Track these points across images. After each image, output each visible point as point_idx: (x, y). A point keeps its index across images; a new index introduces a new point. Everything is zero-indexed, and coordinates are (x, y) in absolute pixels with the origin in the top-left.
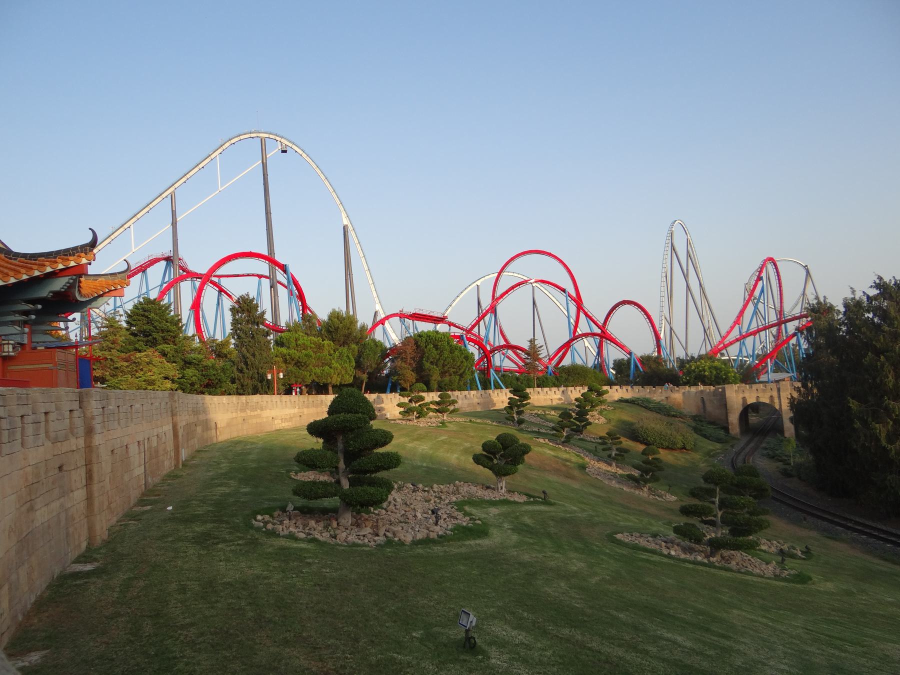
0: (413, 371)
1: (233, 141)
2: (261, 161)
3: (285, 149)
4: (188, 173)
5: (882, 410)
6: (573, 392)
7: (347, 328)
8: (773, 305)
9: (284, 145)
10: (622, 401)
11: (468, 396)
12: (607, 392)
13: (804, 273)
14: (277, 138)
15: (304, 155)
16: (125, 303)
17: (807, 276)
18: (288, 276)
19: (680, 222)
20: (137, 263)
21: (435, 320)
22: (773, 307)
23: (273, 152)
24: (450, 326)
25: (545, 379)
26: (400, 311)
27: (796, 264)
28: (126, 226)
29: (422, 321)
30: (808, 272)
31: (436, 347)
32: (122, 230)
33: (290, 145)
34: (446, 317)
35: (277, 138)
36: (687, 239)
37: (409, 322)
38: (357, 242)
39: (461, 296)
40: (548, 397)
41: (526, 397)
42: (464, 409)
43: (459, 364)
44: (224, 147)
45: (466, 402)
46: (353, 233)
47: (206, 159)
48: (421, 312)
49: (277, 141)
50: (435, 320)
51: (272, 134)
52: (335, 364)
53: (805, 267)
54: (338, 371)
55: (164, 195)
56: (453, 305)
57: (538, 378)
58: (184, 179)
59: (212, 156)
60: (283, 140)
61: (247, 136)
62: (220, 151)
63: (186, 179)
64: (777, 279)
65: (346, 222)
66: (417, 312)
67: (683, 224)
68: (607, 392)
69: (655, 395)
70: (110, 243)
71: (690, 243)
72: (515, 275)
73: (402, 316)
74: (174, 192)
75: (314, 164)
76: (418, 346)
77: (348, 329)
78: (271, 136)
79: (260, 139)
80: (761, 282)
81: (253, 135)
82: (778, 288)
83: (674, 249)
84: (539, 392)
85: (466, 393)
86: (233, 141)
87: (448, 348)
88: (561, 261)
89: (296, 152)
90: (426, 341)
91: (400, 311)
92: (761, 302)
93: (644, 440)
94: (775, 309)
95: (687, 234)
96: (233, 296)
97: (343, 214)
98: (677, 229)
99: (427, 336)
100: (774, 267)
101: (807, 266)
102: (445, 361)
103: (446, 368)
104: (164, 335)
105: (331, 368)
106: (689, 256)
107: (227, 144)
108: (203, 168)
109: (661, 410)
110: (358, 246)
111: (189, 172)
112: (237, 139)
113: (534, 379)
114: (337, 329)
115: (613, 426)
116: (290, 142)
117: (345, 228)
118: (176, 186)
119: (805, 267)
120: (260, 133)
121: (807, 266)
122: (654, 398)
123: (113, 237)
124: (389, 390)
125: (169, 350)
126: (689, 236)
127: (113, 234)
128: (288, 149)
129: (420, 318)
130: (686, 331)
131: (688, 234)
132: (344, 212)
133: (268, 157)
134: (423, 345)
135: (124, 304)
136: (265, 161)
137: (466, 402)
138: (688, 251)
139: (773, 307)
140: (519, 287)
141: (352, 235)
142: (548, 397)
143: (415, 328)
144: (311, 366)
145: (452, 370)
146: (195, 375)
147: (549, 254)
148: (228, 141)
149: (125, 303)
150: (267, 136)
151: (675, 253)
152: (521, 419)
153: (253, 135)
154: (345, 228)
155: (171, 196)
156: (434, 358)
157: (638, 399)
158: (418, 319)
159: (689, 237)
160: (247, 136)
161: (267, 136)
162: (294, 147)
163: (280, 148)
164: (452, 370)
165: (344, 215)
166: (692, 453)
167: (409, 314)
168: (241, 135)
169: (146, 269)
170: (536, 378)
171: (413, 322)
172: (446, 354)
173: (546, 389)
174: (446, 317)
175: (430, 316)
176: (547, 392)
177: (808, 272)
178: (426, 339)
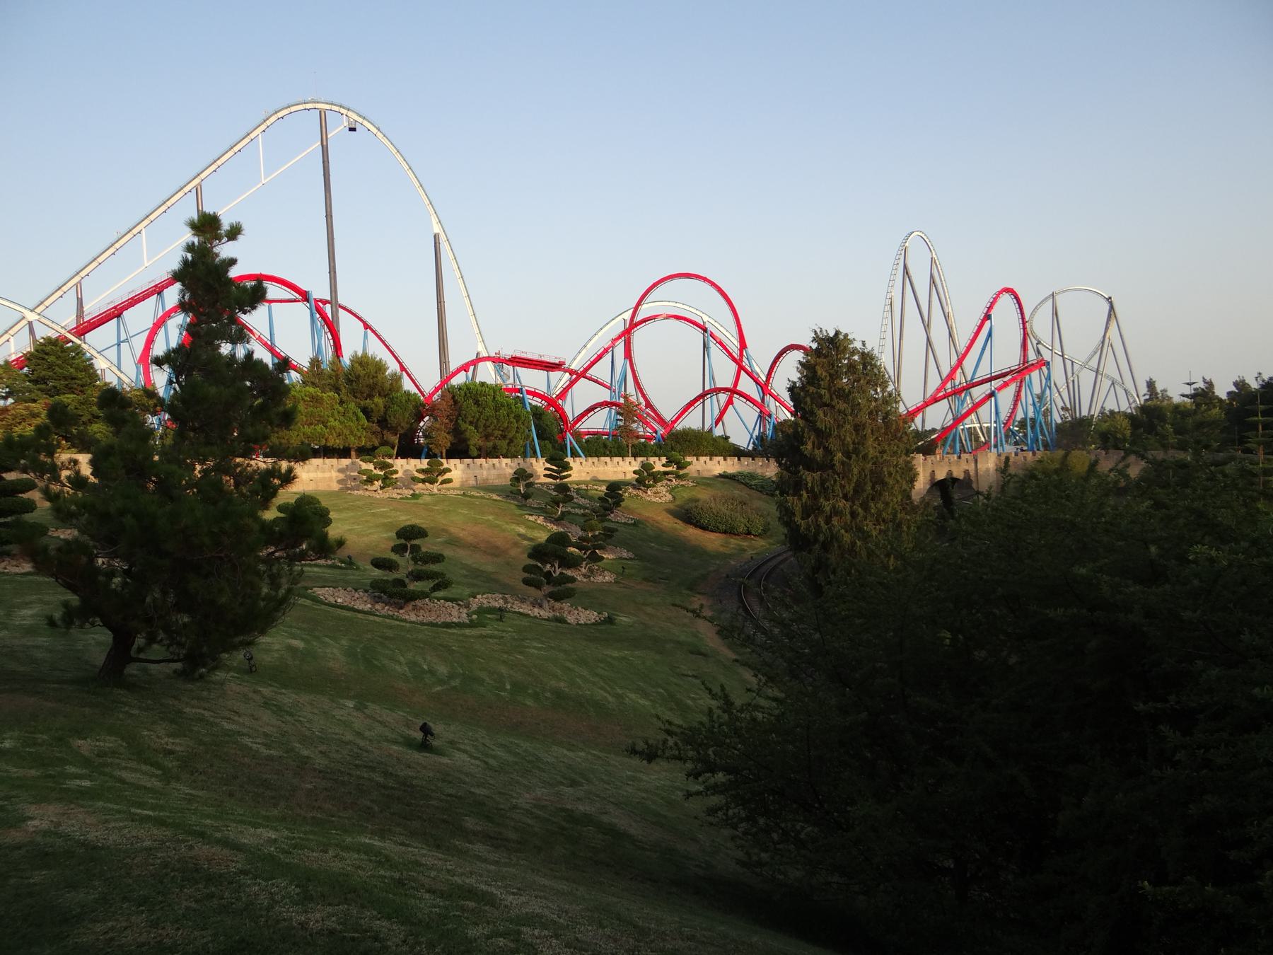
0: (448, 433)
1: (280, 115)
2: (319, 143)
3: (353, 126)
4: (219, 159)
5: (276, 481)
6: (583, 464)
7: (371, 377)
8: (608, 357)
9: (352, 120)
10: (724, 476)
11: (497, 465)
12: (690, 463)
13: (1107, 307)
14: (343, 111)
15: (379, 135)
16: (132, 337)
17: (1110, 311)
18: (310, 305)
19: (920, 234)
20: (150, 282)
21: (546, 367)
22: (1060, 353)
23: (337, 130)
24: (570, 374)
25: (643, 447)
26: (496, 354)
27: (1094, 295)
28: (135, 231)
29: (527, 367)
30: (1112, 307)
31: (477, 403)
32: (130, 236)
33: (360, 120)
34: (564, 363)
35: (343, 111)
36: (932, 258)
37: (508, 369)
38: (451, 256)
39: (600, 334)
40: (619, 469)
41: (566, 467)
42: (491, 482)
43: (506, 425)
44: (268, 123)
45: (494, 472)
46: (446, 244)
47: (243, 139)
48: (523, 356)
49: (342, 114)
50: (546, 367)
51: (335, 105)
52: (332, 423)
53: (1107, 299)
54: (338, 431)
55: (186, 190)
56: (588, 346)
57: (633, 445)
58: (213, 167)
59: (253, 136)
60: (350, 114)
61: (301, 107)
62: (263, 127)
63: (216, 167)
64: (1020, 317)
65: (437, 229)
66: (518, 355)
67: (925, 238)
68: (690, 463)
69: (768, 470)
70: (114, 254)
71: (935, 262)
72: (678, 305)
73: (498, 360)
74: (200, 184)
75: (393, 148)
76: (456, 402)
77: (374, 377)
78: (334, 108)
79: (318, 111)
80: (989, 321)
81: (308, 106)
82: (1022, 330)
83: (907, 273)
84: (606, 462)
85: (495, 461)
86: (280, 115)
87: (492, 404)
88: (713, 284)
89: (369, 130)
90: (466, 395)
91: (496, 354)
92: (748, 398)
93: (697, 522)
94: (1063, 356)
95: (931, 251)
96: (254, 330)
97: (433, 218)
98: (914, 244)
99: (468, 389)
100: (1015, 302)
101: (1110, 298)
102: (487, 420)
103: (489, 430)
104: (67, 383)
105: (326, 427)
106: (933, 282)
107: (273, 119)
108: (240, 151)
109: (764, 488)
110: (454, 263)
111: (221, 157)
112: (286, 112)
113: (628, 446)
114: (358, 377)
115: (676, 506)
116: (360, 116)
117: (436, 237)
118: (203, 176)
119: (1107, 299)
120: (318, 103)
121: (1110, 298)
122: (767, 474)
123: (117, 246)
124: (423, 456)
125: (69, 401)
126: (934, 254)
127: (117, 241)
128: (358, 127)
129: (535, 365)
130: (925, 387)
131: (933, 251)
132: (435, 215)
133: (329, 136)
134: (460, 399)
135: (130, 337)
136: (325, 143)
137: (494, 472)
138: (932, 276)
139: (1060, 353)
140: (644, 324)
141: (444, 247)
142: (619, 469)
143: (517, 376)
144: (299, 424)
145: (497, 433)
146: (100, 432)
147: (705, 279)
148: (274, 114)
149: (132, 337)
150: (328, 107)
151: (909, 277)
152: (35, 483)
153: (308, 106)
154: (436, 237)
155: (197, 189)
156: (474, 417)
157: (740, 474)
158: (521, 364)
159: (934, 256)
160: (301, 107)
161: (328, 107)
162: (365, 123)
163: (346, 124)
164: (497, 433)
165: (434, 220)
166: (760, 540)
167: (507, 357)
168: (279, 111)
169: (163, 291)
170: (630, 445)
171: (514, 369)
172: (489, 412)
173: (616, 459)
174: (564, 363)
175: (520, 358)
176: (618, 462)
177: (1112, 307)
178: (465, 393)
